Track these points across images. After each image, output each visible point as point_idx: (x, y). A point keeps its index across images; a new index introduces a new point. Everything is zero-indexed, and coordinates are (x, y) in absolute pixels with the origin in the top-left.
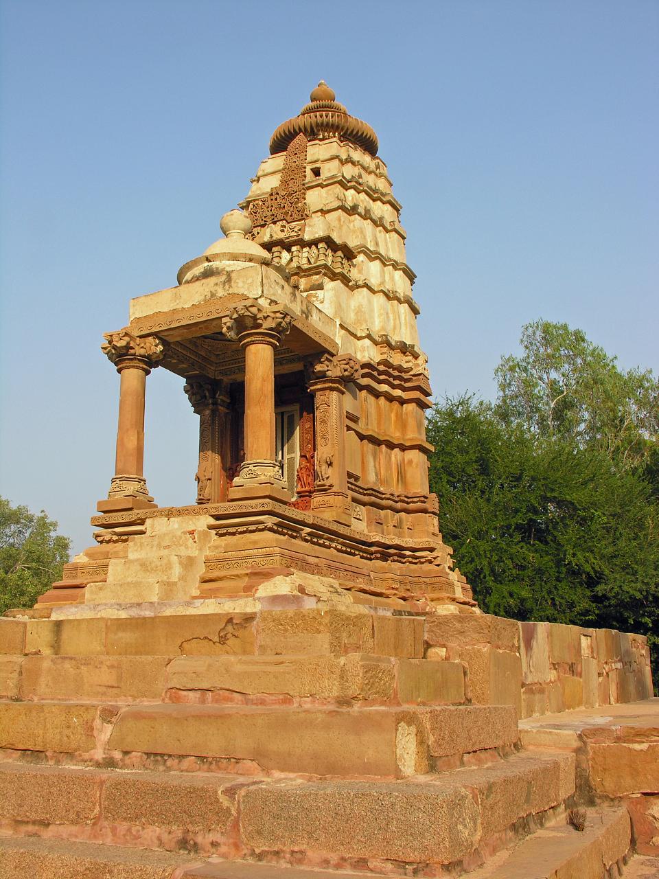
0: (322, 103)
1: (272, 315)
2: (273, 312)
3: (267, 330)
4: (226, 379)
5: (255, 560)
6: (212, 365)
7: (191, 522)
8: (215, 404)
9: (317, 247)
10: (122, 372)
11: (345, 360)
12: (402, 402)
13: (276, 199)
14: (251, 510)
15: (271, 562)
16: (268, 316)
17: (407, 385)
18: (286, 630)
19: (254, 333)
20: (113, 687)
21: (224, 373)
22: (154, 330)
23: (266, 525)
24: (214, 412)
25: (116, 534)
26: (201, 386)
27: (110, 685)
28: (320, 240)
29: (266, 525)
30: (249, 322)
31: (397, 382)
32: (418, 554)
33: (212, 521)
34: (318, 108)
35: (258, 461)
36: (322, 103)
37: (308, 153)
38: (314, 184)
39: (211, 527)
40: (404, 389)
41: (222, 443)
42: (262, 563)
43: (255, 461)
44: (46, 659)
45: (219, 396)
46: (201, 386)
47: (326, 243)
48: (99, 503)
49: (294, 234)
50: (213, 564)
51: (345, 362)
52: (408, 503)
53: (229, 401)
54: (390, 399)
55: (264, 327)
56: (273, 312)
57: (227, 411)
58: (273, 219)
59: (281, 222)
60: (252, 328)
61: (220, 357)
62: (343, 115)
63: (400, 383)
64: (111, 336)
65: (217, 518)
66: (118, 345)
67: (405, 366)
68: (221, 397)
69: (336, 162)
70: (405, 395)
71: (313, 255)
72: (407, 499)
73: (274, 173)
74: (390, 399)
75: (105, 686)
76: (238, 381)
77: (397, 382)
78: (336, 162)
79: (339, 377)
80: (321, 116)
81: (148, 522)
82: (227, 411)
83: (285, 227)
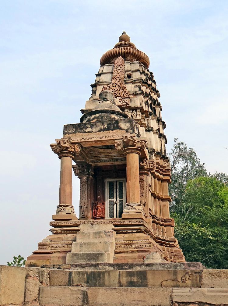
1: (141, 141)
2: (141, 140)
3: (137, 147)
4: (93, 164)
5: (140, 245)
6: (88, 157)
7: (104, 227)
8: (89, 174)
9: (136, 111)
10: (61, 158)
11: (152, 162)
12: (163, 181)
14: (134, 224)
15: (148, 246)
16: (139, 142)
17: (164, 173)
21: (93, 162)
22: (79, 141)
23: (141, 230)
25: (64, 230)
26: (83, 167)
28: (138, 108)
29: (141, 230)
30: (131, 143)
31: (161, 172)
32: (171, 243)
33: (113, 227)
35: (136, 203)
37: (125, 67)
38: (129, 81)
39: (113, 229)
40: (164, 175)
41: (91, 192)
42: (144, 246)
43: (134, 203)
44: (172, 285)
46: (83, 167)
48: (53, 216)
51: (152, 163)
52: (165, 222)
54: (159, 179)
55: (137, 146)
56: (141, 140)
58: (115, 96)
60: (131, 146)
61: (92, 154)
63: (162, 172)
65: (116, 226)
66: (63, 146)
67: (164, 165)
68: (91, 172)
69: (139, 73)
70: (164, 178)
72: (165, 221)
73: (108, 73)
74: (159, 179)
76: (98, 165)
77: (161, 172)
78: (139, 73)
79: (149, 169)
80: (124, 49)
81: (81, 226)
83: (121, 100)
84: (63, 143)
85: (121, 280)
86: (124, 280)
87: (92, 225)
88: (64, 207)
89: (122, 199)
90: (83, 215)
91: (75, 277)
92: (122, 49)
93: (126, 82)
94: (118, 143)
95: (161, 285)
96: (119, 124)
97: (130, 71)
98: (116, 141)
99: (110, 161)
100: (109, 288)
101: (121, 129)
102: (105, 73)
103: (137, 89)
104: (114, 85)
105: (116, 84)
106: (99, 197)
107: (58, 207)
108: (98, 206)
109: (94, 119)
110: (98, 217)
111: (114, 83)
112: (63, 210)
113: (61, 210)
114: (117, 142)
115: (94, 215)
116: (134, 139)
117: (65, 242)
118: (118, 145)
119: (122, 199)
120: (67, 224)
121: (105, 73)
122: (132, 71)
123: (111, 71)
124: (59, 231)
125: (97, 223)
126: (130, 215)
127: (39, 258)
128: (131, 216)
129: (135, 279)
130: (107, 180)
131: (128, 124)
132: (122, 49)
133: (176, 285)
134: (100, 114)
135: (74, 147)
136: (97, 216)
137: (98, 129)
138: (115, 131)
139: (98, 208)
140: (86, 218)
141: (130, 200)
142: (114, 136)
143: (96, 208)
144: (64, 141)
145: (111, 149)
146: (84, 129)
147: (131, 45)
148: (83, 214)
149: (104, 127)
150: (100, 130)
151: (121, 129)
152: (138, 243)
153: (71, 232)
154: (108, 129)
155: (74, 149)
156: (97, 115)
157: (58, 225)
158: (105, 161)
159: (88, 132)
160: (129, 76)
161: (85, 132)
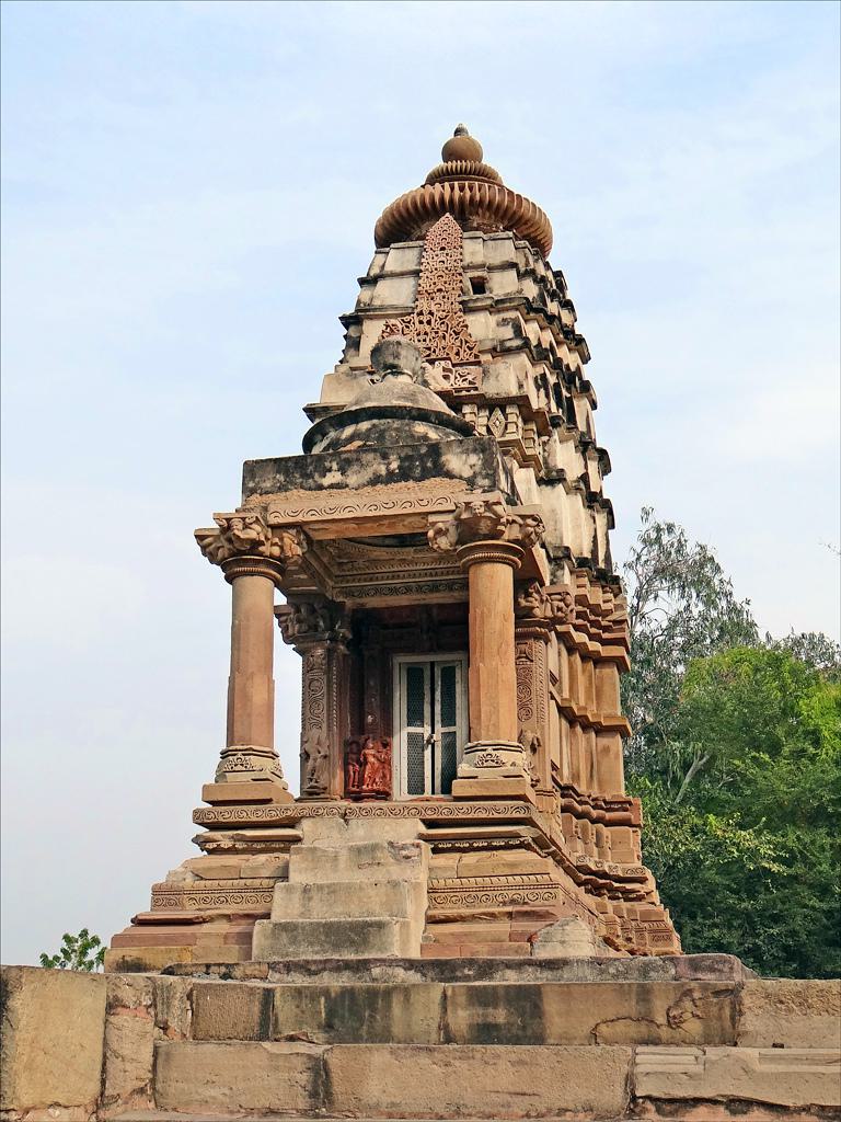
0: (461, 162)
3: (509, 541)
4: (349, 603)
9: (503, 411)
11: (559, 594)
12: (599, 661)
13: (429, 322)
14: (496, 816)
15: (546, 896)
16: (514, 521)
17: (606, 636)
18: (790, 1010)
19: (486, 545)
20: (524, 1094)
21: (349, 593)
22: (300, 518)
23: (522, 839)
24: (330, 652)
25: (243, 839)
27: (518, 1090)
28: (511, 401)
29: (522, 839)
30: (484, 527)
32: (629, 886)
33: (422, 829)
34: (470, 173)
36: (461, 162)
38: (479, 304)
39: (421, 837)
40: (604, 642)
42: (531, 897)
45: (340, 627)
47: (519, 407)
48: (205, 788)
49: (466, 385)
50: (443, 895)
52: (607, 810)
53: (350, 637)
55: (506, 536)
57: (347, 652)
58: (429, 355)
59: (442, 362)
60: (486, 537)
61: (345, 567)
62: (496, 187)
64: (228, 520)
65: (430, 824)
67: (604, 607)
68: (342, 631)
69: (513, 273)
70: (606, 651)
71: (498, 423)
72: (609, 806)
73: (402, 274)
75: (510, 1093)
78: (513, 273)
80: (462, 189)
81: (306, 825)
82: (347, 652)
83: (451, 371)
84: (240, 526)
85: (450, 1019)
86: (461, 1018)
87: (346, 820)
88: (243, 757)
89: (452, 729)
90: (313, 784)
91: (284, 1009)
92: (452, 188)
93: (467, 309)
94: (440, 525)
95: (594, 1036)
96: (443, 458)
97: (482, 266)
98: (432, 519)
99: (408, 590)
101: (450, 475)
102: (393, 275)
103: (508, 332)
104: (425, 319)
105: (431, 313)
107: (225, 755)
109: (351, 439)
110: (366, 791)
111: (425, 310)
112: (239, 768)
113: (235, 768)
114: (433, 524)
115: (353, 786)
116: (495, 513)
117: (249, 882)
118: (439, 532)
119: (452, 729)
120: (254, 819)
121: (393, 275)
122: (491, 269)
123: (414, 267)
124: (226, 844)
125: (364, 813)
126: (482, 785)
127: (156, 940)
128: (487, 788)
129: (500, 1015)
130: (401, 660)
131: (474, 459)
132: (452, 188)
134: (375, 421)
135: (281, 539)
136: (364, 787)
137: (367, 474)
139: (365, 759)
140: (322, 796)
143: (358, 762)
144: (244, 519)
145: (412, 549)
146: (316, 476)
147: (487, 176)
148: (311, 780)
149: (387, 469)
150: (376, 481)
151: (450, 475)
152: (510, 887)
153: (268, 845)
154: (404, 475)
155: (282, 548)
156: (364, 426)
157: (221, 820)
158: (394, 591)
159: (332, 486)
160: (479, 286)
161: (320, 487)
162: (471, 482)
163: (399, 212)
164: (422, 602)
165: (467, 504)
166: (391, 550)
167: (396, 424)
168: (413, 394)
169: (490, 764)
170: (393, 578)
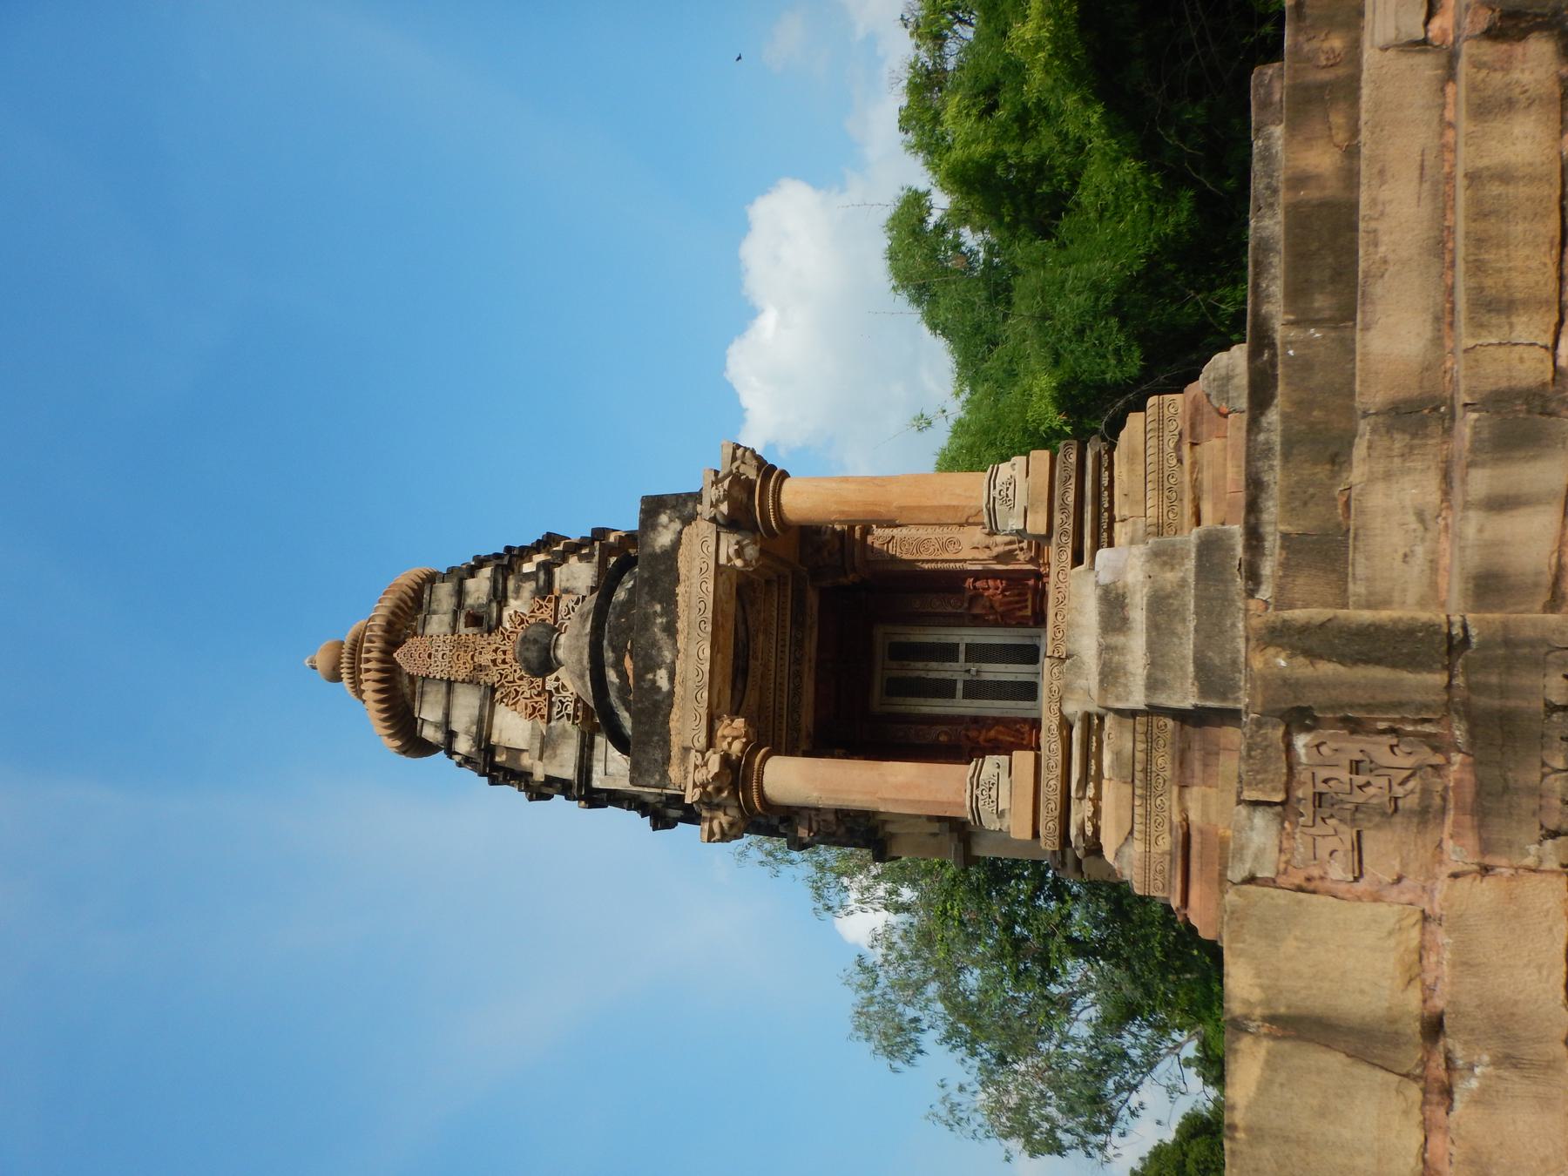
1: (737, 463)
22: (703, 711)
25: (1083, 783)
84: (704, 770)
85: (1326, 314)
87: (1068, 657)
92: (368, 670)
94: (731, 551)
96: (658, 550)
97: (455, 613)
98: (723, 560)
99: (798, 675)
100: (1363, 312)
101: (677, 543)
103: (529, 586)
104: (500, 656)
105: (495, 651)
106: (943, 738)
108: (981, 739)
109: (622, 674)
111: (490, 656)
112: (993, 793)
113: (994, 797)
114: (729, 559)
116: (725, 477)
117: (1138, 767)
118: (739, 553)
120: (1059, 771)
122: (460, 605)
123: (444, 687)
132: (368, 670)
133: (1371, 594)
134: (605, 643)
135: (724, 737)
137: (661, 636)
138: (683, 570)
139: (989, 741)
141: (973, 503)
142: (704, 566)
144: (696, 767)
145: (751, 662)
146: (659, 697)
149: (661, 616)
151: (677, 543)
152: (1161, 450)
154: (670, 600)
155: (735, 738)
156: (609, 655)
157: (1057, 813)
158: (797, 691)
159: (672, 679)
161: (671, 693)
162: (688, 520)
163: (382, 711)
164: (813, 664)
165: (712, 505)
166: (749, 684)
167: (611, 618)
168: (581, 616)
169: (1010, 492)
170: (782, 690)
